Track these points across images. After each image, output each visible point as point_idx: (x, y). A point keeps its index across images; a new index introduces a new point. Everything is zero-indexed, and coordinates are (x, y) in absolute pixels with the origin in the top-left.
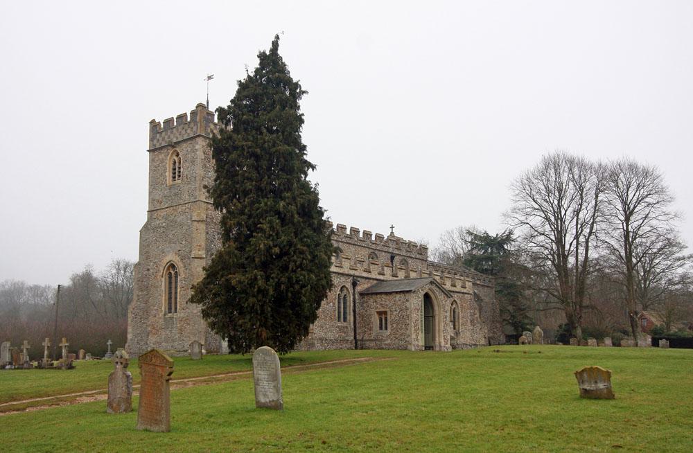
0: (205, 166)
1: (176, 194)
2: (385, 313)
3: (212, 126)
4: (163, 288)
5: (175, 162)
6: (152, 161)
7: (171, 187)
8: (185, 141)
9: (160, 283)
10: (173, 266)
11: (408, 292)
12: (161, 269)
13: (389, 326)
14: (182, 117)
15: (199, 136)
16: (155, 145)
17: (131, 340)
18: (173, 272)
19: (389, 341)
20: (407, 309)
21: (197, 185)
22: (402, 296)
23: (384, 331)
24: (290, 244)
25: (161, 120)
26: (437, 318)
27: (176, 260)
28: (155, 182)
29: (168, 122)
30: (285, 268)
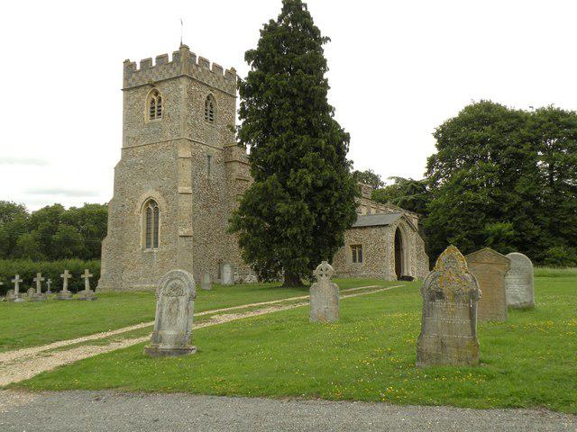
0: (188, 105)
1: (155, 132)
2: (360, 246)
3: (194, 67)
4: (141, 224)
5: (153, 101)
6: (126, 99)
7: (149, 125)
8: (166, 81)
9: (137, 218)
10: (152, 202)
11: (384, 226)
12: (139, 205)
13: (364, 259)
14: (162, 59)
15: (183, 76)
16: (130, 85)
17: (105, 275)
18: (152, 208)
19: (364, 273)
20: (383, 242)
21: (181, 124)
22: (378, 230)
23: (358, 263)
24: (332, 179)
25: (136, 59)
26: (405, 250)
27: (156, 196)
28: (130, 121)
29: (146, 63)
30: (327, 200)
